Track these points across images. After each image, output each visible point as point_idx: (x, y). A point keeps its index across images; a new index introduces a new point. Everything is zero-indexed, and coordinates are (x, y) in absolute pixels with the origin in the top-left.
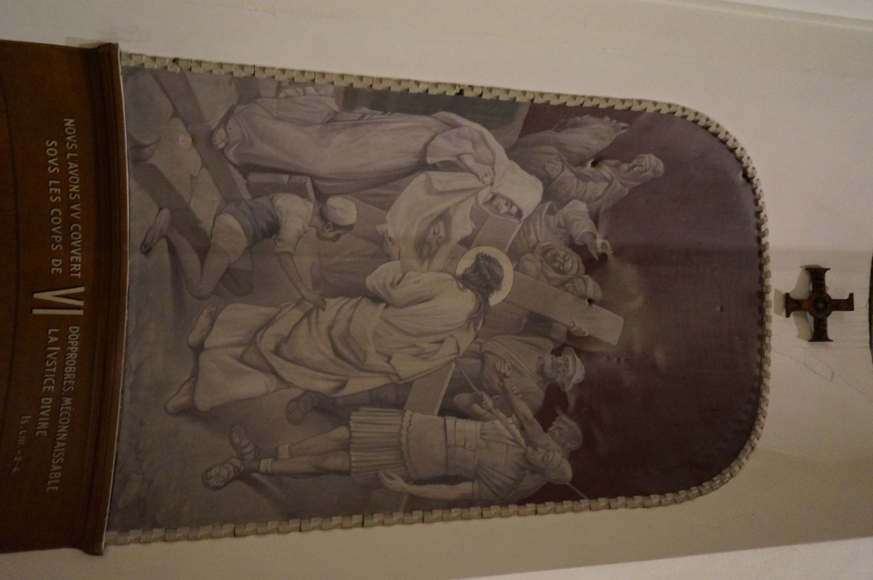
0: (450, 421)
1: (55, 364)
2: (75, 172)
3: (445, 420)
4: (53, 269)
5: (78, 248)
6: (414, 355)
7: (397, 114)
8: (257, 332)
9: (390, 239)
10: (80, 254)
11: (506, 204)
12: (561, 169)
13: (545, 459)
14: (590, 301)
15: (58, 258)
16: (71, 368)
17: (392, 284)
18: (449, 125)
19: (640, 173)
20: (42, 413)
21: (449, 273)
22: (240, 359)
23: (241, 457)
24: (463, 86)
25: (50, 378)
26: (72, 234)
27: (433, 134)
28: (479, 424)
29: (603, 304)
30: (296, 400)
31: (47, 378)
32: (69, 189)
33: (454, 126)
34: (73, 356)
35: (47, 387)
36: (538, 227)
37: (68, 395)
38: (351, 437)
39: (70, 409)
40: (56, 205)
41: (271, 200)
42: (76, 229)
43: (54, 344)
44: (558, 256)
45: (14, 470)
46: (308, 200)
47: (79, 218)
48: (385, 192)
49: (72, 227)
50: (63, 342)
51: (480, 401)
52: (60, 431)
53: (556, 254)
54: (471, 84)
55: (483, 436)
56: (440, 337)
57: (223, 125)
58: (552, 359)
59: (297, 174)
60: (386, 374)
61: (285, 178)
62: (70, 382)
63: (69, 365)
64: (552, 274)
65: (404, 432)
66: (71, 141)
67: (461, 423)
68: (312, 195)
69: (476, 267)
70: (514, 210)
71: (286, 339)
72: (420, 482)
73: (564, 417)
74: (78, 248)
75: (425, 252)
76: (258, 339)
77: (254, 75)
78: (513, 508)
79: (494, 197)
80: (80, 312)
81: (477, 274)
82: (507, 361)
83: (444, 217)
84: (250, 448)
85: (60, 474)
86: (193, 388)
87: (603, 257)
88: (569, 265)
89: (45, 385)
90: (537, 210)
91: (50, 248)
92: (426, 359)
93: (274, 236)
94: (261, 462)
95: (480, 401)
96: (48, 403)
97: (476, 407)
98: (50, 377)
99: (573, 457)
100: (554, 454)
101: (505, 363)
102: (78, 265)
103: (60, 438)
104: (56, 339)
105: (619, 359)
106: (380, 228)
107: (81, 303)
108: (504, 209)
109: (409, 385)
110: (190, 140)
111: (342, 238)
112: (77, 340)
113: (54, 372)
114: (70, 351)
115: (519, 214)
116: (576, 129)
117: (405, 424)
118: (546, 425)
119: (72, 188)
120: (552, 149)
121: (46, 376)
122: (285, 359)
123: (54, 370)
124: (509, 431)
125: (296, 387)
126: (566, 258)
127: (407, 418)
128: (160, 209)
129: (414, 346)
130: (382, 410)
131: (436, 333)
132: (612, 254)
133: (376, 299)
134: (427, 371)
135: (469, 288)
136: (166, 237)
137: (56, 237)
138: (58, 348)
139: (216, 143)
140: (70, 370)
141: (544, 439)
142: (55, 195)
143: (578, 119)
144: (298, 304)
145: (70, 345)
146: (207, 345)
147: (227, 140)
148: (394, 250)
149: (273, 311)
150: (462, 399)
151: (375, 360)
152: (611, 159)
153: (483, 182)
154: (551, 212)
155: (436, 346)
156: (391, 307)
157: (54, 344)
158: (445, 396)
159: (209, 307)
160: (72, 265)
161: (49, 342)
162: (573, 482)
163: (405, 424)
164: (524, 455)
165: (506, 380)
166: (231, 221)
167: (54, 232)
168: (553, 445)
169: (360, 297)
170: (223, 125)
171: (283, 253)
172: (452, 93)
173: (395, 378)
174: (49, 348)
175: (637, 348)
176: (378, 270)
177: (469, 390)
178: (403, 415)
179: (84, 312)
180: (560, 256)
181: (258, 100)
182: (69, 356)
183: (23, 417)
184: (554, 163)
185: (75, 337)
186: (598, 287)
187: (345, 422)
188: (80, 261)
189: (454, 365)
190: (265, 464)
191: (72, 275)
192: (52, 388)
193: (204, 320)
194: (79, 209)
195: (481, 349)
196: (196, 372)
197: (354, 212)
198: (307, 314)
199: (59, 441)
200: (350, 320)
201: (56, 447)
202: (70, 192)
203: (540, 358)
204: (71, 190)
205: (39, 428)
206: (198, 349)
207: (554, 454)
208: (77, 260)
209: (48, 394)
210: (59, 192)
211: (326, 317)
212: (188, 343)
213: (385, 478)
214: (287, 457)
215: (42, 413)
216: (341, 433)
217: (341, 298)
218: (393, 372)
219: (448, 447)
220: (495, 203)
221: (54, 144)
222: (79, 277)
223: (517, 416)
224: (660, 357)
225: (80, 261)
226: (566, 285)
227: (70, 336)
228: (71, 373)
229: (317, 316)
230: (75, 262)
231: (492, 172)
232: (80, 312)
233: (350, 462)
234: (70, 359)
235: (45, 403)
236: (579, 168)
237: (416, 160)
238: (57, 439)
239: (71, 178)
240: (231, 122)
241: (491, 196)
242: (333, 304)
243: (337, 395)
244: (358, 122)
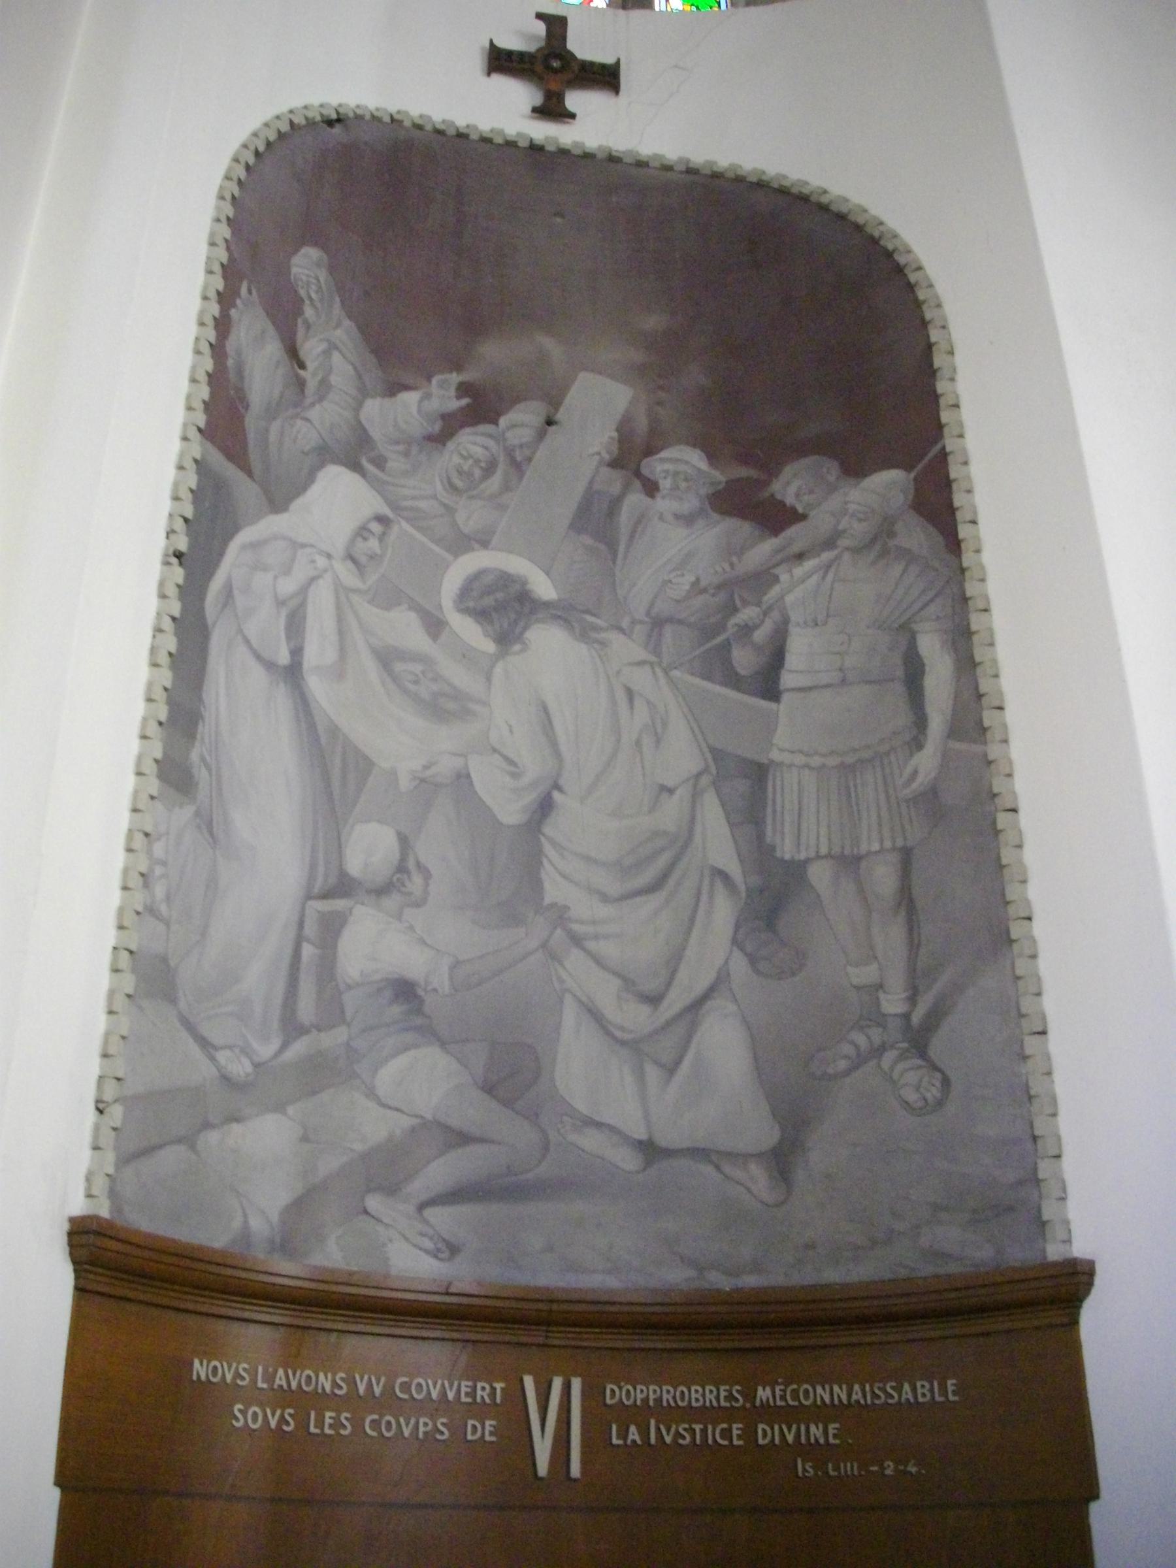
0: (788, 679)
1: (687, 1426)
2: (294, 1375)
3: (788, 690)
4: (488, 1438)
5: (443, 1385)
6: (658, 741)
7: (204, 696)
8: (609, 1033)
9: (426, 767)
10: (456, 1383)
11: (365, 539)
12: (309, 425)
13: (862, 516)
14: (550, 422)
15: (466, 1426)
16: (694, 1395)
17: (515, 776)
18: (225, 605)
19: (319, 290)
20: (790, 1438)
21: (493, 666)
22: (671, 1070)
23: (879, 1051)
24: (167, 548)
25: (715, 1434)
26: (416, 1396)
27: (239, 637)
28: (794, 630)
29: (554, 399)
30: (753, 960)
33: (228, 592)
34: (667, 1394)
35: (326, 1426)
36: (406, 492)
37: (750, 1395)
38: (829, 856)
39: (782, 1387)
40: (358, 1424)
41: (349, 987)
42: (406, 1387)
43: (644, 1432)
44: (461, 467)
45: (914, 1470)
46: (351, 913)
47: (383, 1379)
48: (338, 761)
50: (640, 1414)
51: (747, 630)
52: (827, 1400)
53: (458, 471)
54: (164, 535)
55: (819, 623)
56: (621, 696)
57: (210, 1050)
58: (663, 497)
59: (301, 924)
60: (696, 795)
61: (308, 951)
62: (723, 1394)
63: (687, 1398)
64: (495, 482)
65: (816, 761)
67: (793, 660)
68: (339, 904)
69: (482, 615)
70: (376, 527)
71: (628, 983)
72: (921, 722)
73: (776, 487)
74: (443, 1385)
75: (451, 706)
76: (627, 1036)
77: (131, 952)
78: (967, 559)
79: (351, 557)
80: (576, 1384)
81: (493, 614)
82: (666, 578)
83: (387, 658)
84: (861, 1039)
85: (919, 1384)
86: (732, 1156)
87: (464, 389)
88: (478, 451)
89: (731, 1440)
90: (378, 486)
91: (444, 1441)
92: (665, 724)
93: (420, 992)
94: (886, 1012)
95: (747, 630)
96: (314, 1379)
97: (760, 636)
98: (773, 1433)
99: (855, 470)
100: (850, 502)
101: (670, 581)
102: (479, 1387)
103: (844, 1397)
104: (633, 1429)
105: (661, 388)
106: (405, 783)
107: (557, 1383)
108: (373, 544)
109: (713, 750)
110: (234, 1126)
111: (422, 859)
112: (635, 1389)
113: (701, 1426)
114: (659, 1400)
115: (381, 519)
116: (246, 373)
117: (799, 759)
118: (795, 517)
119: (323, 1388)
120: (275, 426)
121: (710, 1442)
122: (669, 984)
123: (698, 1427)
124: (809, 577)
125: (726, 962)
126: (465, 453)
127: (786, 758)
128: (366, 1212)
129: (638, 743)
130: (770, 803)
131: (614, 702)
132: (458, 374)
133: (545, 807)
134: (688, 721)
135: (522, 633)
136: (421, 1207)
137: (422, 1429)
138: (653, 1422)
139: (242, 1073)
140: (700, 1395)
141: (821, 521)
142: (337, 1425)
143: (230, 362)
144: (555, 957)
145: (646, 1400)
146: (641, 1134)
147: (237, 1051)
148: (446, 766)
149: (570, 1014)
150: (744, 660)
151: (670, 814)
152: (295, 334)
153: (325, 571)
154: (380, 462)
155: (638, 703)
156: (561, 782)
157: (644, 1432)
158: (738, 689)
159: (562, 1131)
160: (479, 1399)
161: (639, 1442)
162: (908, 468)
163: (799, 759)
164: (856, 551)
165: (703, 583)
166: (387, 1077)
167: (411, 1434)
168: (834, 502)
169: (543, 839)
170: (210, 1050)
171: (451, 978)
172: (178, 574)
173: (705, 780)
174: (653, 1441)
175: (637, 356)
176: (489, 801)
177: (726, 646)
178: (780, 764)
180: (459, 464)
181: (172, 964)
182: (668, 1401)
183: (800, 1474)
184: (298, 432)
185: (628, 1391)
186: (522, 406)
187: (796, 871)
189: (676, 673)
190: (893, 1004)
191: (498, 1400)
192: (736, 1430)
193: (591, 1141)
194: (794, 1427)
195: (641, 622)
196: (699, 1153)
197: (373, 828)
198: (577, 941)
199: (849, 1396)
200: (588, 859)
201: (862, 1402)
202: (872, 1402)
203: (661, 518)
204: (328, 1389)
205: (822, 1441)
206: (650, 1150)
207: (850, 502)
208: (469, 1390)
209: (750, 1434)
210: (333, 1414)
211: (583, 907)
212: (638, 1172)
213: (914, 785)
214: (875, 966)
215: (790, 1438)
216: (820, 875)
217: (543, 875)
218: (691, 782)
219: (844, 682)
220: (363, 560)
221: (240, 1411)
223: (778, 565)
224: (654, 322)
225: (470, 1383)
226: (519, 459)
227: (626, 1402)
228: (704, 1395)
229: (582, 922)
230: (472, 1394)
231: (308, 550)
233: (881, 851)
234: (674, 1398)
235: (425, 1388)
236: (307, 392)
237: (282, 685)
238: (845, 1402)
239: (305, 1388)
240: (206, 1030)
241: (350, 564)
242: (555, 890)
243: (742, 888)
244: (214, 773)
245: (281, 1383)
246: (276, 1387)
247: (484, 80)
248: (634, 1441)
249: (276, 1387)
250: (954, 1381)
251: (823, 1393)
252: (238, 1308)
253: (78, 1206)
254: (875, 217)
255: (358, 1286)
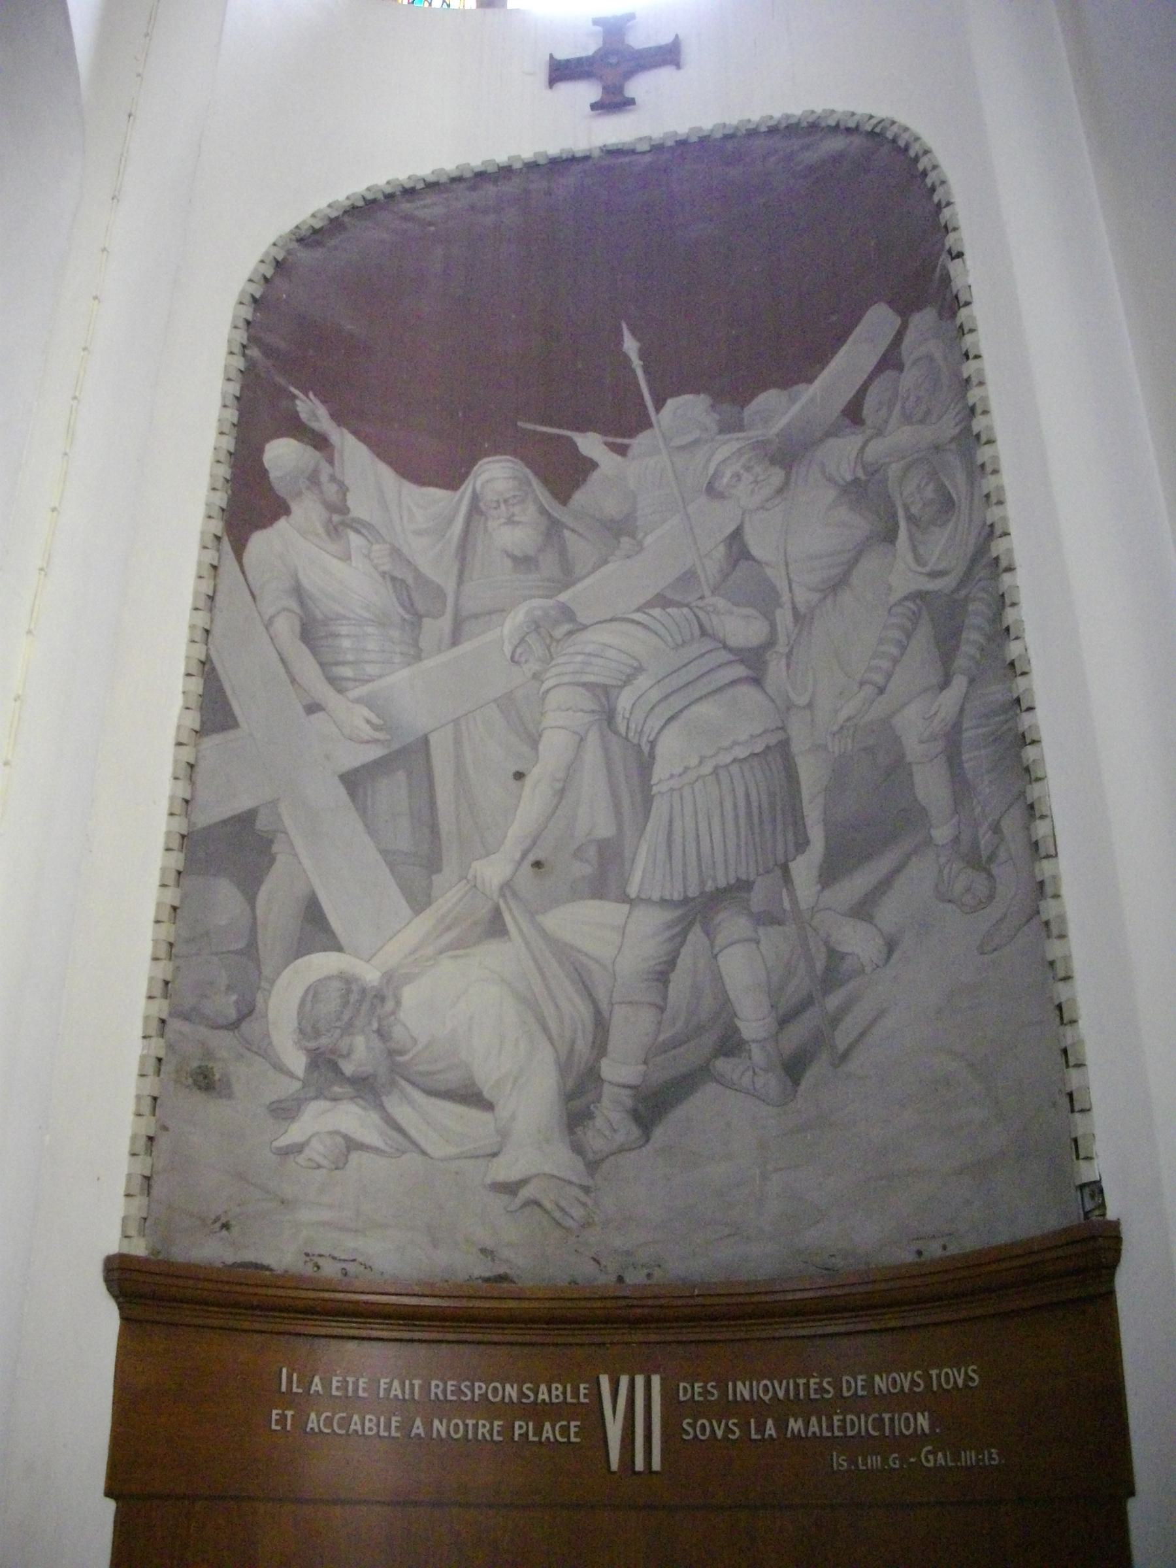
15: (678, 1389)
31: (867, 1430)
32: (513, 1402)
35: (572, 1435)
49: (876, 1434)
66: (911, 1383)
80: (656, 1380)
96: (853, 1385)
98: (860, 1424)
107: (624, 1381)
119: (510, 1397)
123: (470, 1422)
179: (655, 1373)
188: (455, 1383)
205: (441, 1397)
222: (420, 1382)
232: (656, 1380)
239: (892, 1391)
245: (770, 1432)
246: (392, 1396)
247: (548, 94)
248: (771, 1435)
249: (392, 1396)
250: (501, 1423)
251: (743, 1388)
252: (347, 1328)
253: (112, 1244)
254: (862, 115)
255: (512, 1299)
